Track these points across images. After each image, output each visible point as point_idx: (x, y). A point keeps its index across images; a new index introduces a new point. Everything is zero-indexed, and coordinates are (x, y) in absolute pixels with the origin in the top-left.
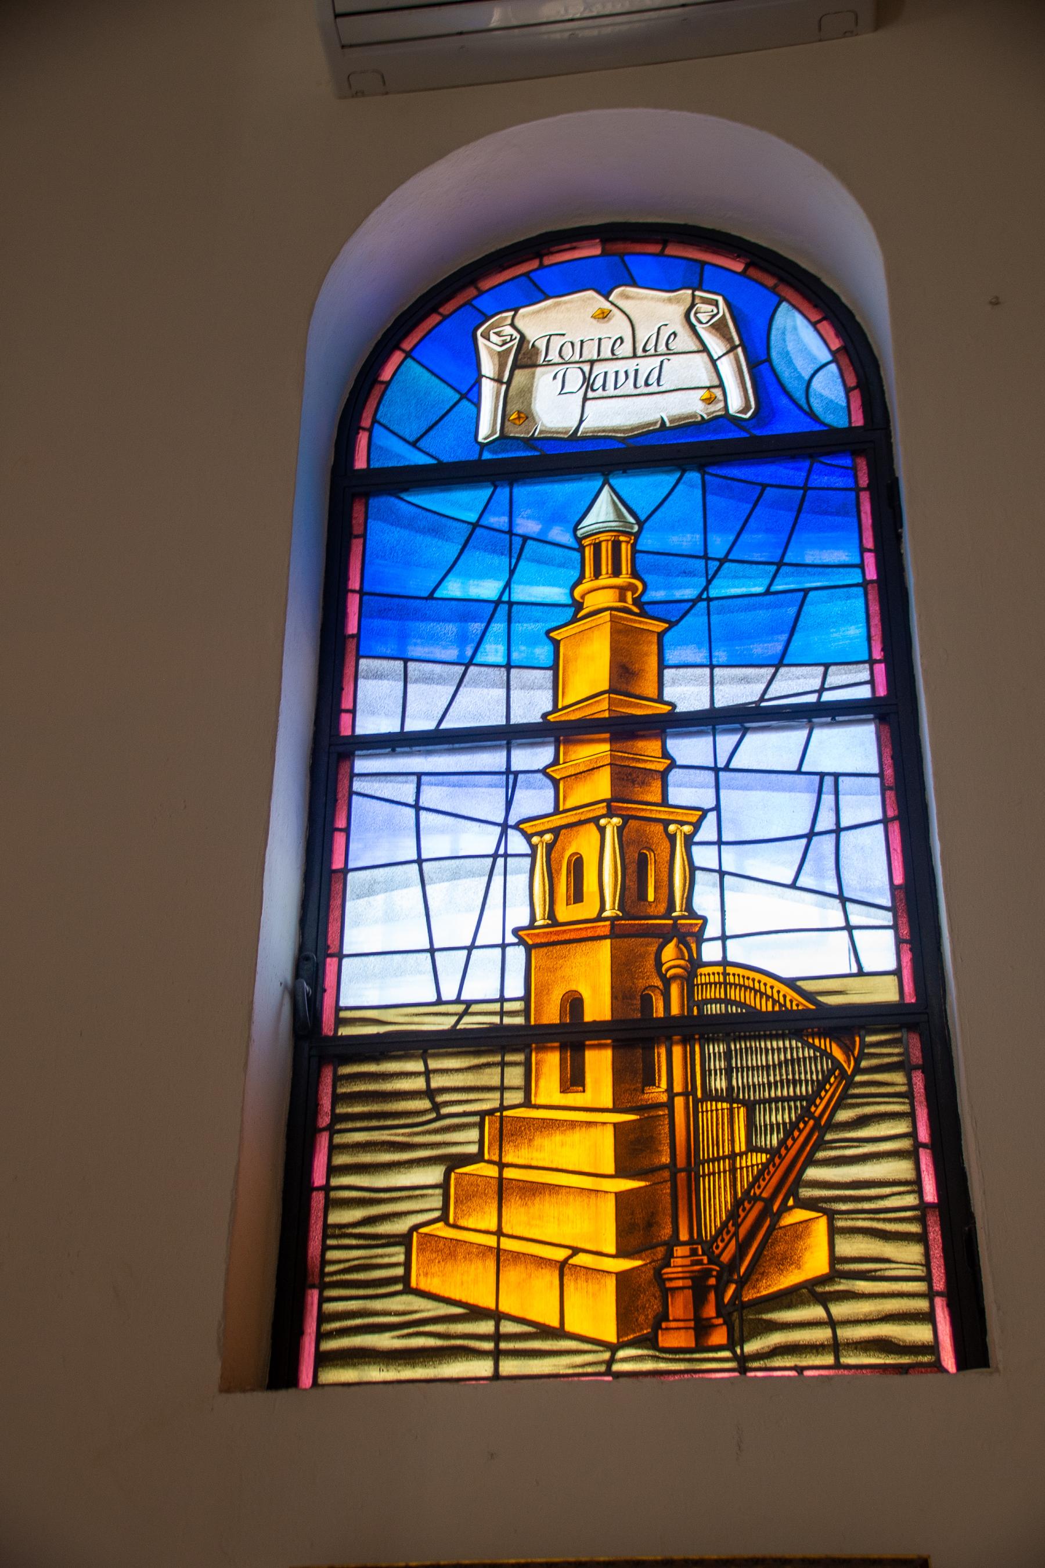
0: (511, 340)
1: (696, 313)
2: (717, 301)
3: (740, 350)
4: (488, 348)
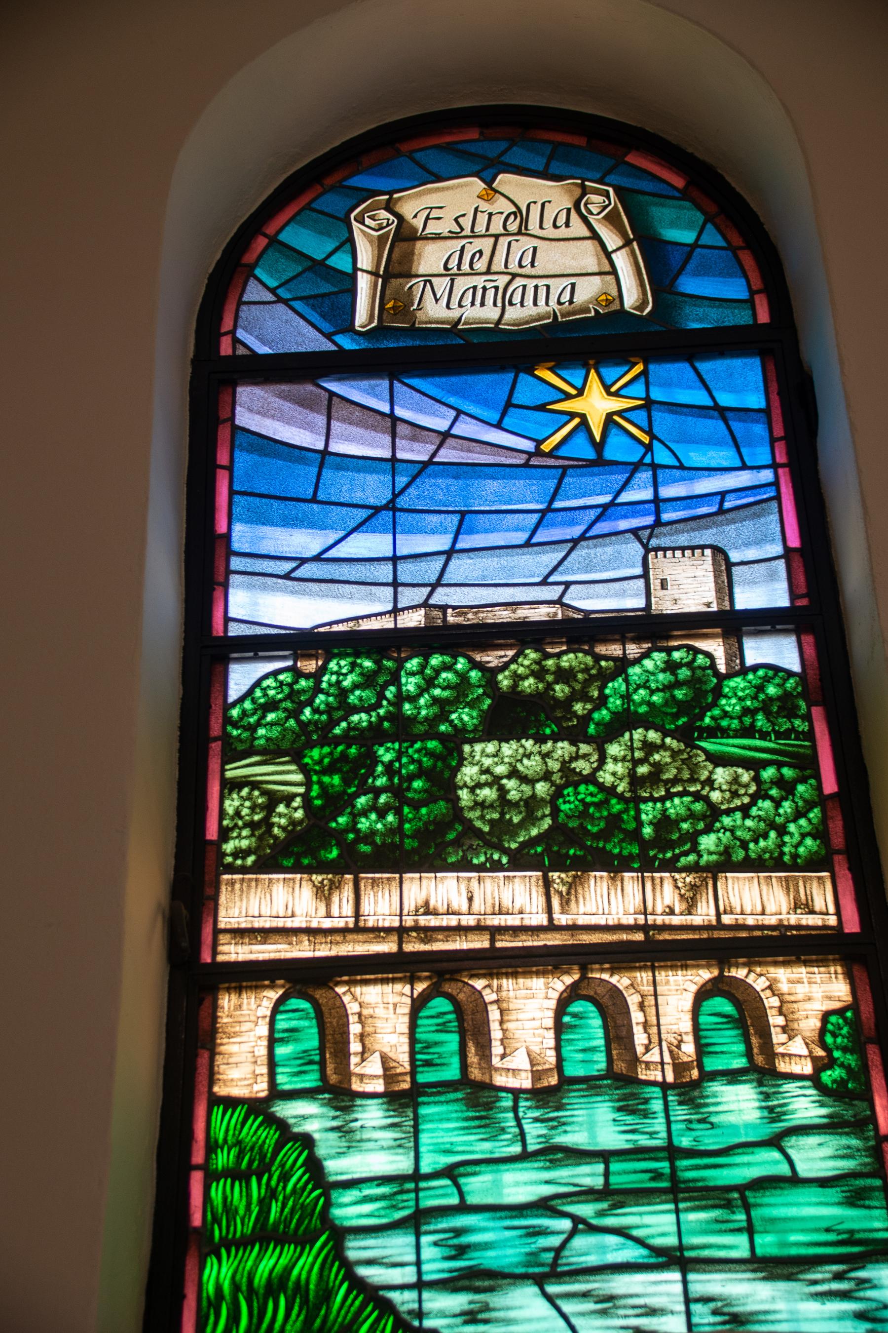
0: (388, 225)
1: (586, 205)
2: (608, 192)
3: (635, 244)
4: (362, 231)
